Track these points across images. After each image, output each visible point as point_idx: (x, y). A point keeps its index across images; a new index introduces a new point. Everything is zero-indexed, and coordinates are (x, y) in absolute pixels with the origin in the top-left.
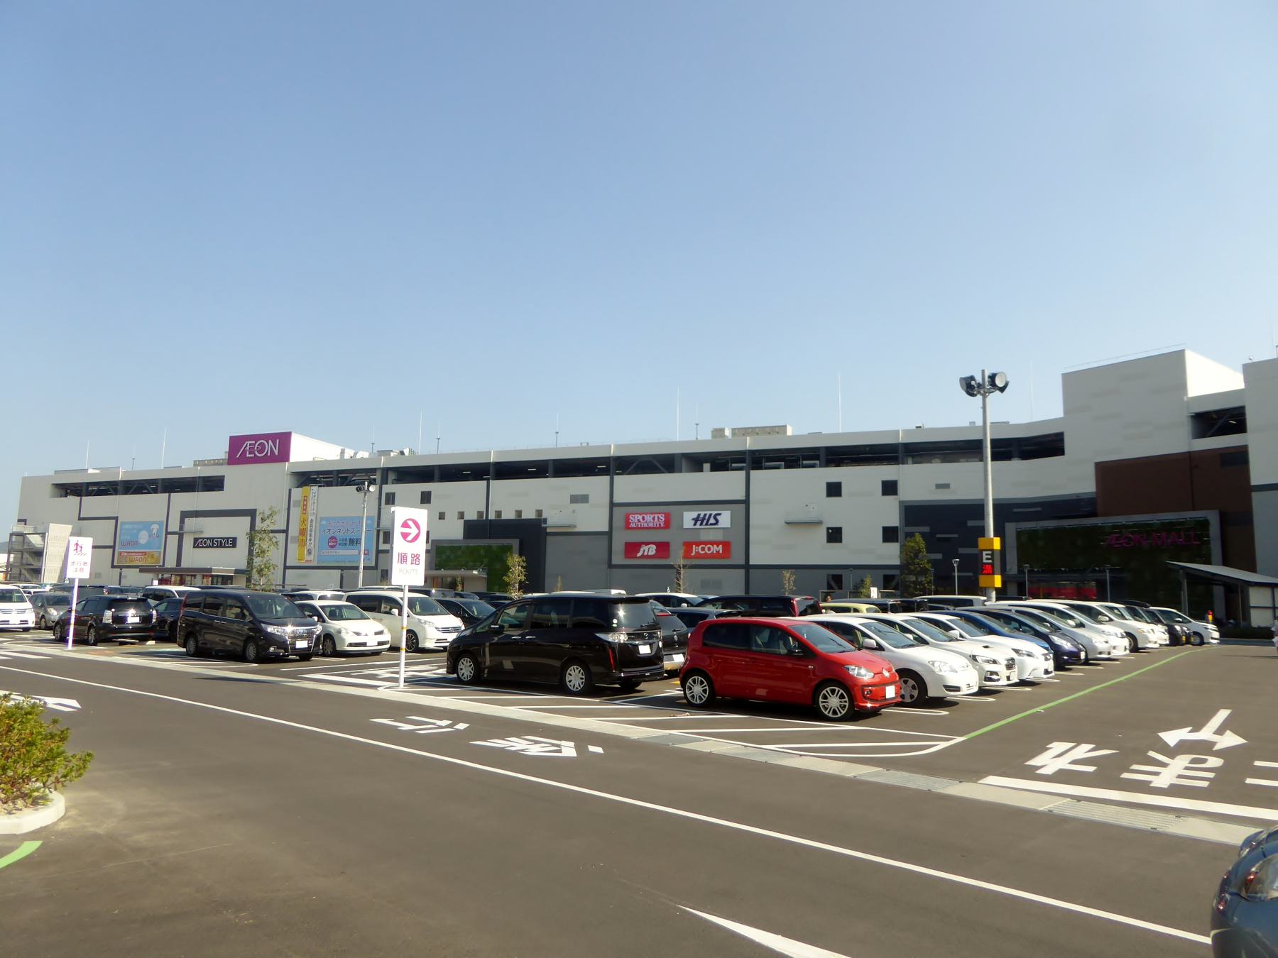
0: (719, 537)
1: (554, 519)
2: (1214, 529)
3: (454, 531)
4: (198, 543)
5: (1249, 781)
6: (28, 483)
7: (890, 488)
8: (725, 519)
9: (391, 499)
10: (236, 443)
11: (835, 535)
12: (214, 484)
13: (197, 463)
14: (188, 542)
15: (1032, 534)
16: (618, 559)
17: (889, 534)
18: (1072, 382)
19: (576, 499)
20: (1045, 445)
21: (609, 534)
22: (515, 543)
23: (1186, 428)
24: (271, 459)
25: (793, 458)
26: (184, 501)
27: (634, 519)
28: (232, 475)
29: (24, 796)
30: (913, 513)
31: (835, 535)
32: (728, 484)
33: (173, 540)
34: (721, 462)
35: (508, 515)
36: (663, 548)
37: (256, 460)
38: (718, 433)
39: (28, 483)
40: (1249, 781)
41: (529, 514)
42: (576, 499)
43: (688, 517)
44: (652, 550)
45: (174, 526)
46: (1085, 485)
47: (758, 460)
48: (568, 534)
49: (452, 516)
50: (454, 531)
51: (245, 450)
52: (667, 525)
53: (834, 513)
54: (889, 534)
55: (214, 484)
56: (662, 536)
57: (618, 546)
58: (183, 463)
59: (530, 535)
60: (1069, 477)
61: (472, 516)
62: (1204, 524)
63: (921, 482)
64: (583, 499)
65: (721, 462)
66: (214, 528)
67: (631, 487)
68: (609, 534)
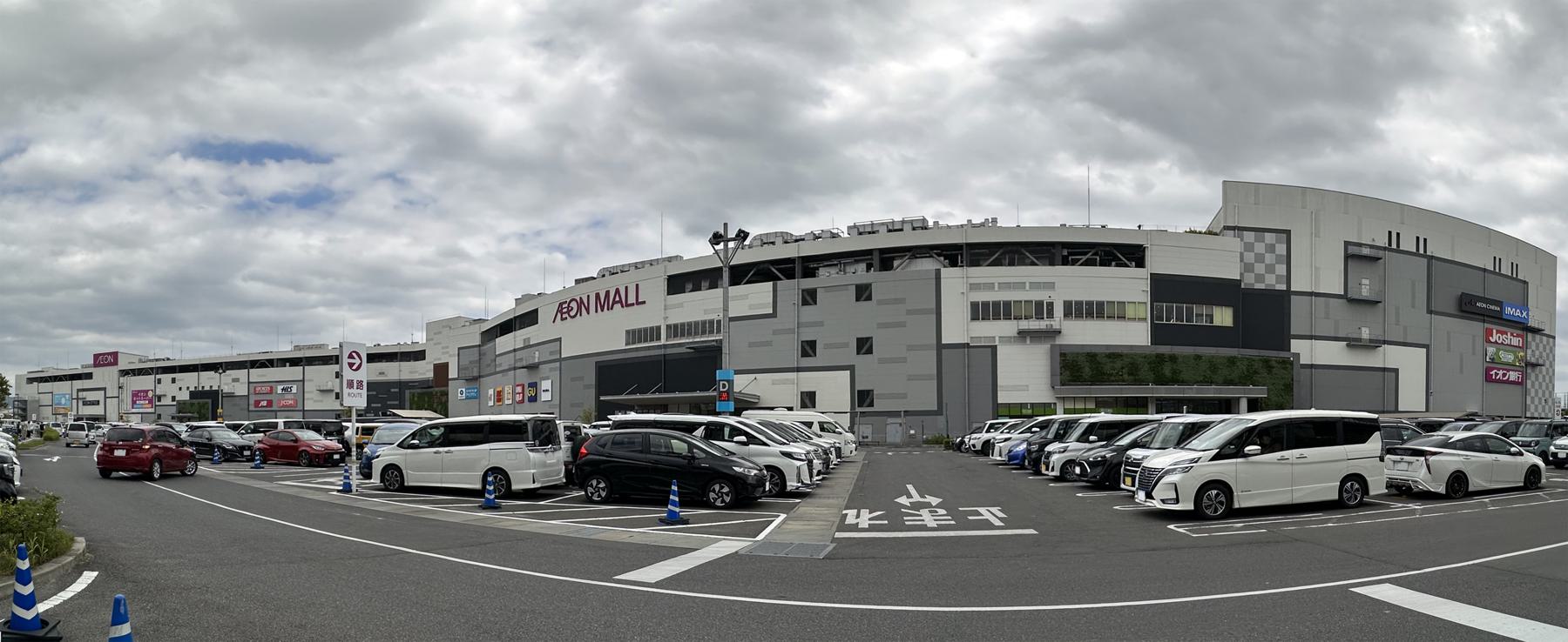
1: (226, 389)
3: (184, 396)
4: (85, 403)
12: (89, 376)
26: (78, 384)
28: (96, 372)
34: (295, 362)
36: (270, 403)
43: (280, 388)
47: (311, 361)
48: (231, 396)
50: (184, 396)
51: (105, 360)
52: (271, 392)
56: (269, 397)
57: (252, 402)
64: (236, 380)
65: (295, 362)
66: (91, 396)
67: (257, 374)
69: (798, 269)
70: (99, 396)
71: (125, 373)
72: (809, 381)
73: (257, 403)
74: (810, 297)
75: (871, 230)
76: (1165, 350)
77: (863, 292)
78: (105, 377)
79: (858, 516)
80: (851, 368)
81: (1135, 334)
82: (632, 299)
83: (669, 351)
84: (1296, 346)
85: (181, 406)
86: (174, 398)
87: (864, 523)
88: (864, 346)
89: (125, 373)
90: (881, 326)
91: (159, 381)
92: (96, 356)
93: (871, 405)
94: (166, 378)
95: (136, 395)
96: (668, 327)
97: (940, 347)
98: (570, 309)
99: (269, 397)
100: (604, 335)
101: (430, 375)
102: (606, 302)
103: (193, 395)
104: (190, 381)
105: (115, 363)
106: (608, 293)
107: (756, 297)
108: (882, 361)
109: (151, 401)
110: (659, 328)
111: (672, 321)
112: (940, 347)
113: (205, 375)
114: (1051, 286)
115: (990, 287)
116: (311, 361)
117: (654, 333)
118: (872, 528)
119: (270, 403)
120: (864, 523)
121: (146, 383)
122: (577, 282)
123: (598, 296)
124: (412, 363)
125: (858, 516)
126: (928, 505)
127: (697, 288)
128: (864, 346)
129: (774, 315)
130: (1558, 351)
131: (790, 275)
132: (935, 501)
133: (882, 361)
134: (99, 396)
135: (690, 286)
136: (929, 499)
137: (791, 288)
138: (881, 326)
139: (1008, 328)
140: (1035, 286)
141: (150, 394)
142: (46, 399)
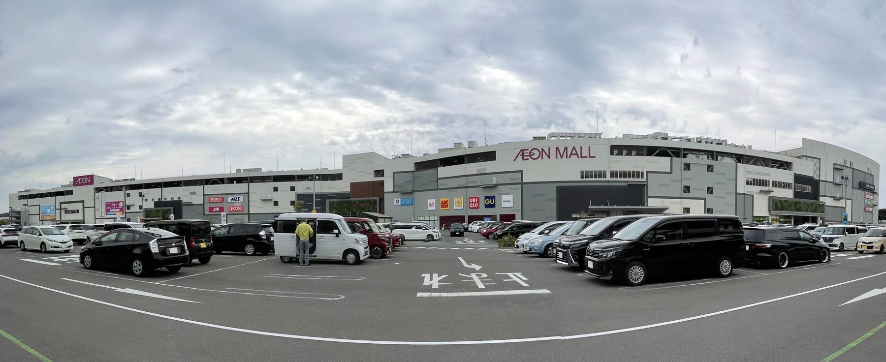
0: (239, 204)
3: (150, 205)
5: (419, 294)
6: (11, 196)
7: (293, 189)
8: (241, 199)
9: (129, 195)
10: (76, 179)
11: (276, 203)
12: (70, 193)
13: (62, 186)
14: (63, 212)
15: (333, 203)
16: (207, 212)
17: (293, 203)
18: (345, 158)
19: (191, 193)
20: (338, 177)
22: (172, 208)
23: (373, 175)
25: (264, 179)
26: (61, 199)
28: (75, 189)
30: (300, 197)
31: (276, 203)
32: (242, 187)
34: (240, 180)
35: (169, 199)
38: (238, 170)
39: (11, 196)
40: (419, 294)
41: (176, 199)
42: (191, 193)
43: (229, 199)
44: (218, 209)
45: (58, 207)
46: (347, 189)
47: (252, 180)
48: (189, 204)
49: (150, 200)
50: (150, 205)
51: (78, 181)
52: (223, 201)
53: (276, 196)
55: (70, 193)
56: (221, 205)
57: (207, 208)
59: (177, 206)
63: (302, 187)
64: (194, 193)
65: (240, 180)
66: (70, 207)
67: (210, 189)
69: (682, 153)
71: (98, 190)
72: (687, 203)
73: (211, 209)
74: (687, 167)
75: (632, 137)
76: (798, 200)
77: (710, 168)
78: (84, 193)
79: (431, 279)
80: (705, 199)
83: (609, 184)
84: (821, 199)
85: (148, 213)
87: (435, 285)
88: (710, 190)
89: (98, 190)
90: (717, 183)
91: (129, 195)
94: (135, 193)
95: (109, 206)
97: (737, 194)
98: (537, 154)
100: (569, 172)
102: (563, 153)
103: (157, 204)
104: (154, 195)
105: (92, 183)
106: (566, 148)
107: (663, 163)
108: (717, 197)
109: (121, 210)
111: (614, 169)
112: (737, 194)
113: (166, 190)
114: (769, 175)
115: (761, 174)
116: (252, 180)
117: (602, 174)
118: (441, 289)
120: (435, 285)
121: (118, 196)
122: (535, 138)
123: (557, 149)
124: (329, 182)
125: (431, 279)
126: (474, 271)
127: (629, 154)
128: (710, 190)
129: (671, 173)
132: (478, 268)
133: (717, 197)
134: (79, 206)
135: (634, 152)
136: (474, 266)
137: (679, 162)
138: (717, 183)
139: (757, 188)
140: (765, 174)
141: (121, 205)
142: (35, 210)
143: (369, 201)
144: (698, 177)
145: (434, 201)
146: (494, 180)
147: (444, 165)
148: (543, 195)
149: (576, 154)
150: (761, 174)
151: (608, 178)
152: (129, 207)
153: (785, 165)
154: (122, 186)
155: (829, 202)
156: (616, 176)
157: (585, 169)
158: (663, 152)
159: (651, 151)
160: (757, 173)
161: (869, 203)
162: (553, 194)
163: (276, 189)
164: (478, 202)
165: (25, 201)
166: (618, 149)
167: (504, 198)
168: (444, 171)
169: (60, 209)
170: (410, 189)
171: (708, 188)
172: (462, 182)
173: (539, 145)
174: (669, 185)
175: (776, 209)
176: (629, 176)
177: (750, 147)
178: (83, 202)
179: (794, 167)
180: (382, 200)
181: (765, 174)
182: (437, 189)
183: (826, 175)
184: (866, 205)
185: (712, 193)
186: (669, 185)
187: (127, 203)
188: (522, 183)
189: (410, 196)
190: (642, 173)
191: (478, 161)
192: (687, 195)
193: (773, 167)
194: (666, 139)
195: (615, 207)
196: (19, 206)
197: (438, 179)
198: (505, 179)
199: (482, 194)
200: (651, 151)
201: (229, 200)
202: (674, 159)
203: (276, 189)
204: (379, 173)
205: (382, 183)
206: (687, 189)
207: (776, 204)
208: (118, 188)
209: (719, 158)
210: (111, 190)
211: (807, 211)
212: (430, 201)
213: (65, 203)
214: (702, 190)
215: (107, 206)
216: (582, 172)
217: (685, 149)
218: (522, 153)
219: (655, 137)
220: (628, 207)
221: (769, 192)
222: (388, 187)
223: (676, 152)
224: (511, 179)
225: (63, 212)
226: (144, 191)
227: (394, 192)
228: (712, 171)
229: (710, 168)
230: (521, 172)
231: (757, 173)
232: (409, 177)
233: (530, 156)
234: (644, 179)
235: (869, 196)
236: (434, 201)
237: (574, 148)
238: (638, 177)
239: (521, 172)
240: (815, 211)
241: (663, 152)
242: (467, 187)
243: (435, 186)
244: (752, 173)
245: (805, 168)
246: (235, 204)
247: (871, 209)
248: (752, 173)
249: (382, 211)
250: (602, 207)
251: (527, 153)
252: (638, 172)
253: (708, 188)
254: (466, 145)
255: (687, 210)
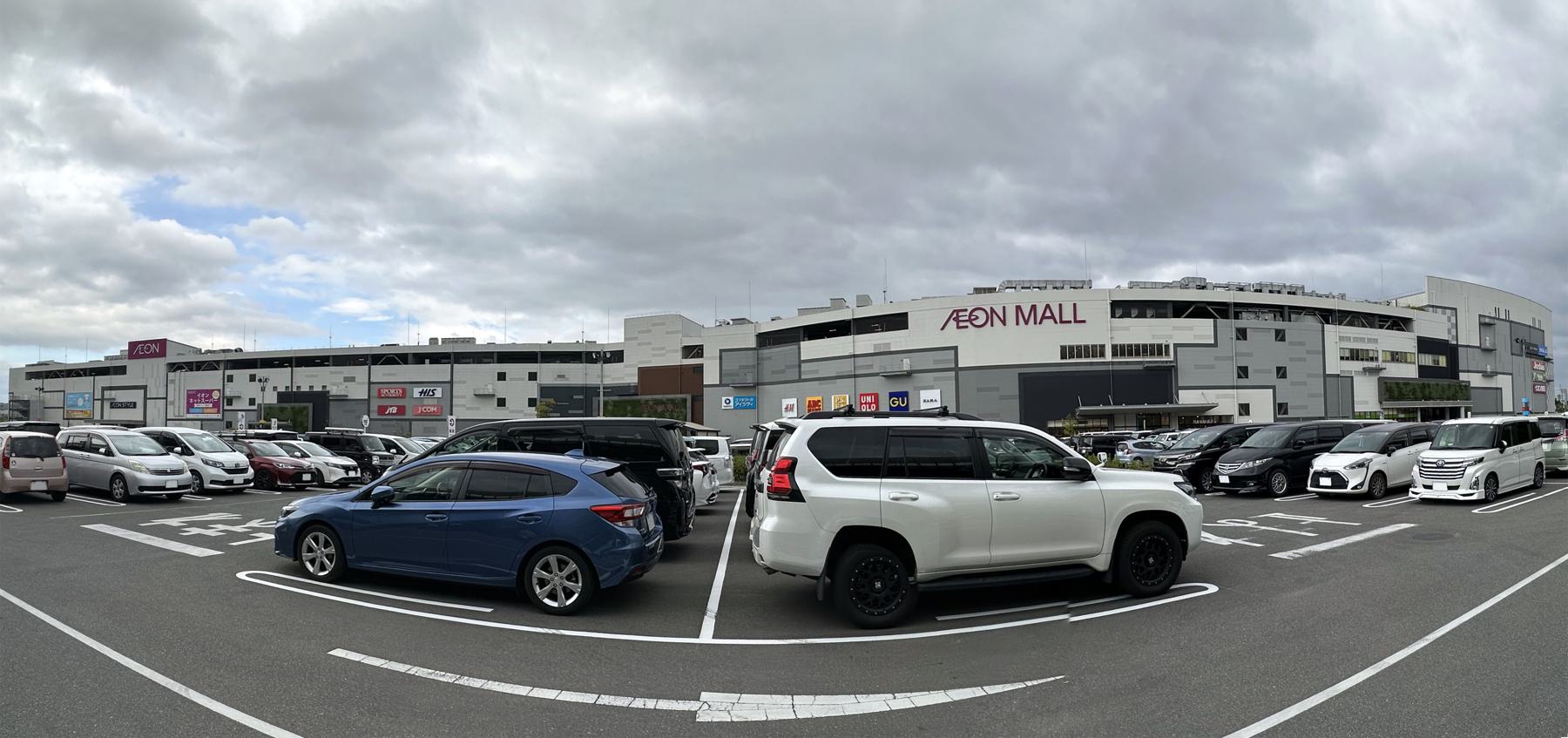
1: (334, 391)
2: (689, 404)
3: (271, 399)
4: (114, 405)
7: (533, 376)
8: (438, 393)
9: (230, 379)
12: (122, 370)
17: (532, 402)
19: (347, 379)
20: (617, 356)
21: (368, 400)
23: (680, 354)
24: (154, 355)
26: (103, 381)
27: (384, 392)
28: (132, 365)
29: (306, 413)
30: (545, 391)
31: (502, 402)
32: (441, 372)
33: (98, 403)
34: (437, 359)
35: (305, 389)
36: (401, 410)
37: (145, 356)
39: (12, 371)
41: (318, 388)
42: (347, 379)
43: (416, 392)
45: (98, 396)
46: (634, 380)
48: (342, 399)
50: (271, 399)
51: (138, 350)
52: (403, 396)
53: (501, 389)
54: (532, 402)
56: (401, 402)
58: (96, 357)
59: (320, 402)
60: (623, 375)
61: (282, 389)
62: (685, 400)
63: (549, 374)
64: (352, 379)
65: (437, 359)
66: (122, 397)
67: (381, 373)
68: (368, 400)
70: (137, 396)
71: (174, 367)
72: (1246, 396)
73: (382, 410)
77: (1280, 335)
80: (1273, 388)
81: (1409, 371)
82: (1068, 315)
83: (1116, 368)
84: (1463, 377)
85: (268, 412)
86: (252, 402)
88: (1281, 372)
89: (174, 367)
91: (230, 379)
92: (133, 345)
93: (1286, 412)
94: (241, 375)
95: (193, 397)
96: (1114, 347)
98: (982, 317)
99: (401, 402)
100: (1040, 348)
101: (634, 380)
104: (280, 378)
105: (162, 354)
106: (1034, 307)
107: (1201, 329)
108: (1292, 384)
109: (216, 404)
110: (1103, 347)
111: (1118, 342)
112: (1326, 376)
113: (301, 372)
114: (1376, 341)
115: (1362, 340)
117: (1099, 350)
119: (401, 410)
121: (210, 380)
123: (1018, 308)
127: (1142, 315)
128: (1281, 372)
129: (1215, 345)
130: (6, 387)
131: (1225, 315)
133: (1292, 384)
134: (137, 396)
135: (1134, 312)
137: (1228, 326)
141: (216, 395)
142: (55, 400)
143: (672, 401)
144: (1262, 349)
145: (793, 401)
146: (906, 364)
147: (810, 338)
148: (997, 389)
149: (1053, 317)
150: (1362, 340)
151: (1109, 357)
152: (230, 401)
153: (1400, 324)
154: (218, 362)
155: (1476, 380)
156: (1123, 354)
157: (1067, 343)
158: (1199, 310)
159: (1180, 309)
160: (1356, 339)
161: (1540, 378)
162: (1014, 388)
163: (502, 376)
164: (877, 402)
165: (38, 383)
166: (1121, 308)
167: (924, 395)
168: (811, 349)
169: (102, 400)
170: (750, 379)
171: (1279, 369)
172: (847, 367)
173: (986, 301)
174: (1212, 367)
175: (1392, 398)
176: (1130, 354)
177: (1343, 296)
178: (145, 388)
179: (1415, 325)
180: (698, 400)
181: (1370, 340)
182: (800, 380)
183: (1469, 335)
184: (1536, 382)
185: (1284, 376)
186: (1212, 367)
187: (228, 393)
188: (957, 369)
189: (753, 393)
190: (1167, 346)
191: (872, 331)
192: (1243, 382)
193: (1381, 327)
194: (1204, 288)
195: (1124, 407)
196: (29, 390)
197: (801, 362)
198: (927, 362)
199: (884, 389)
200: (1180, 309)
201: (416, 395)
202: (1220, 321)
203: (502, 376)
204: (694, 351)
205: (699, 369)
206: (1243, 372)
207: (1391, 390)
208: (211, 366)
209: (1293, 316)
210: (198, 369)
211: (1442, 399)
212: (786, 402)
213: (111, 388)
214: (1270, 371)
215: (189, 396)
216: (1063, 348)
217: (1236, 305)
218: (956, 316)
219: (1184, 284)
220: (1146, 406)
221: (1378, 370)
222: (711, 376)
223: (1219, 311)
224: (936, 362)
225: (107, 405)
226: (260, 373)
227: (721, 385)
228: (1283, 339)
229: (1280, 335)
230: (956, 348)
231: (1356, 339)
232: (750, 359)
233: (970, 320)
234: (1172, 358)
235: (1539, 366)
236: (793, 401)
237: (1048, 306)
238: (1160, 354)
239: (956, 348)
240: (1454, 398)
241: (1199, 310)
242: (855, 376)
243: (797, 374)
244: (1348, 339)
245: (1434, 327)
246: (426, 402)
247: (1543, 389)
248: (1348, 339)
249: (698, 418)
250: (1101, 407)
251: (964, 316)
252: (1160, 346)
253: (1279, 369)
254: (851, 301)
255: (1245, 409)
